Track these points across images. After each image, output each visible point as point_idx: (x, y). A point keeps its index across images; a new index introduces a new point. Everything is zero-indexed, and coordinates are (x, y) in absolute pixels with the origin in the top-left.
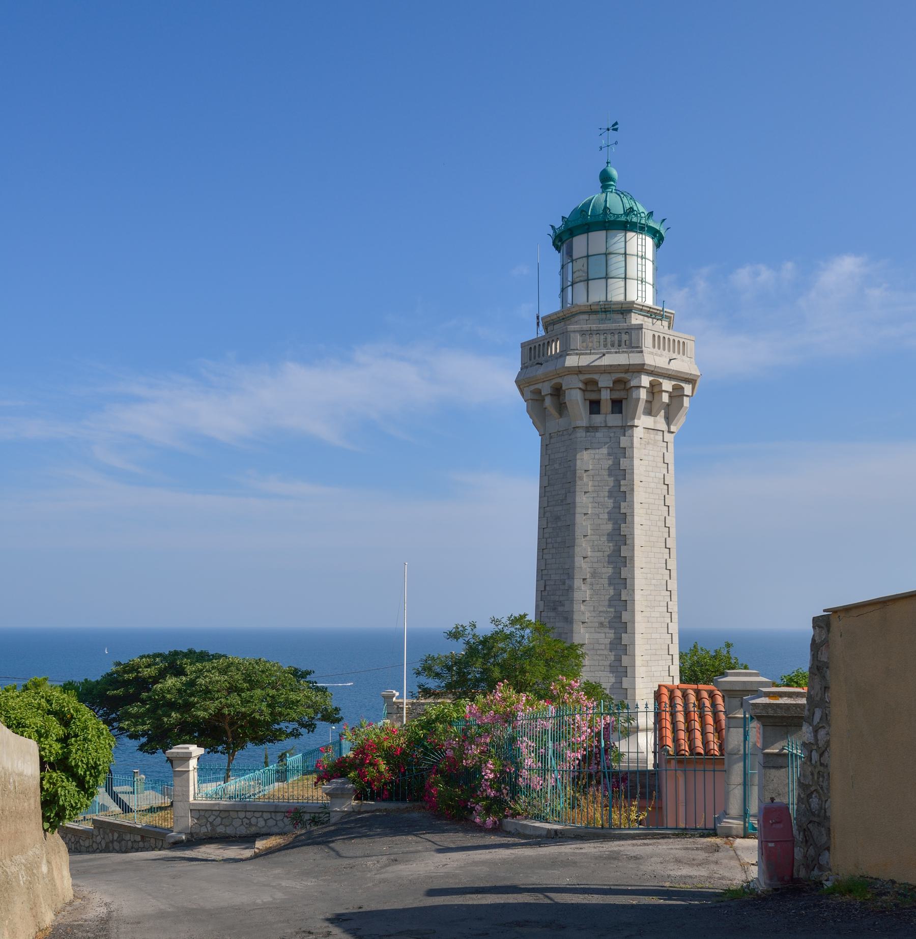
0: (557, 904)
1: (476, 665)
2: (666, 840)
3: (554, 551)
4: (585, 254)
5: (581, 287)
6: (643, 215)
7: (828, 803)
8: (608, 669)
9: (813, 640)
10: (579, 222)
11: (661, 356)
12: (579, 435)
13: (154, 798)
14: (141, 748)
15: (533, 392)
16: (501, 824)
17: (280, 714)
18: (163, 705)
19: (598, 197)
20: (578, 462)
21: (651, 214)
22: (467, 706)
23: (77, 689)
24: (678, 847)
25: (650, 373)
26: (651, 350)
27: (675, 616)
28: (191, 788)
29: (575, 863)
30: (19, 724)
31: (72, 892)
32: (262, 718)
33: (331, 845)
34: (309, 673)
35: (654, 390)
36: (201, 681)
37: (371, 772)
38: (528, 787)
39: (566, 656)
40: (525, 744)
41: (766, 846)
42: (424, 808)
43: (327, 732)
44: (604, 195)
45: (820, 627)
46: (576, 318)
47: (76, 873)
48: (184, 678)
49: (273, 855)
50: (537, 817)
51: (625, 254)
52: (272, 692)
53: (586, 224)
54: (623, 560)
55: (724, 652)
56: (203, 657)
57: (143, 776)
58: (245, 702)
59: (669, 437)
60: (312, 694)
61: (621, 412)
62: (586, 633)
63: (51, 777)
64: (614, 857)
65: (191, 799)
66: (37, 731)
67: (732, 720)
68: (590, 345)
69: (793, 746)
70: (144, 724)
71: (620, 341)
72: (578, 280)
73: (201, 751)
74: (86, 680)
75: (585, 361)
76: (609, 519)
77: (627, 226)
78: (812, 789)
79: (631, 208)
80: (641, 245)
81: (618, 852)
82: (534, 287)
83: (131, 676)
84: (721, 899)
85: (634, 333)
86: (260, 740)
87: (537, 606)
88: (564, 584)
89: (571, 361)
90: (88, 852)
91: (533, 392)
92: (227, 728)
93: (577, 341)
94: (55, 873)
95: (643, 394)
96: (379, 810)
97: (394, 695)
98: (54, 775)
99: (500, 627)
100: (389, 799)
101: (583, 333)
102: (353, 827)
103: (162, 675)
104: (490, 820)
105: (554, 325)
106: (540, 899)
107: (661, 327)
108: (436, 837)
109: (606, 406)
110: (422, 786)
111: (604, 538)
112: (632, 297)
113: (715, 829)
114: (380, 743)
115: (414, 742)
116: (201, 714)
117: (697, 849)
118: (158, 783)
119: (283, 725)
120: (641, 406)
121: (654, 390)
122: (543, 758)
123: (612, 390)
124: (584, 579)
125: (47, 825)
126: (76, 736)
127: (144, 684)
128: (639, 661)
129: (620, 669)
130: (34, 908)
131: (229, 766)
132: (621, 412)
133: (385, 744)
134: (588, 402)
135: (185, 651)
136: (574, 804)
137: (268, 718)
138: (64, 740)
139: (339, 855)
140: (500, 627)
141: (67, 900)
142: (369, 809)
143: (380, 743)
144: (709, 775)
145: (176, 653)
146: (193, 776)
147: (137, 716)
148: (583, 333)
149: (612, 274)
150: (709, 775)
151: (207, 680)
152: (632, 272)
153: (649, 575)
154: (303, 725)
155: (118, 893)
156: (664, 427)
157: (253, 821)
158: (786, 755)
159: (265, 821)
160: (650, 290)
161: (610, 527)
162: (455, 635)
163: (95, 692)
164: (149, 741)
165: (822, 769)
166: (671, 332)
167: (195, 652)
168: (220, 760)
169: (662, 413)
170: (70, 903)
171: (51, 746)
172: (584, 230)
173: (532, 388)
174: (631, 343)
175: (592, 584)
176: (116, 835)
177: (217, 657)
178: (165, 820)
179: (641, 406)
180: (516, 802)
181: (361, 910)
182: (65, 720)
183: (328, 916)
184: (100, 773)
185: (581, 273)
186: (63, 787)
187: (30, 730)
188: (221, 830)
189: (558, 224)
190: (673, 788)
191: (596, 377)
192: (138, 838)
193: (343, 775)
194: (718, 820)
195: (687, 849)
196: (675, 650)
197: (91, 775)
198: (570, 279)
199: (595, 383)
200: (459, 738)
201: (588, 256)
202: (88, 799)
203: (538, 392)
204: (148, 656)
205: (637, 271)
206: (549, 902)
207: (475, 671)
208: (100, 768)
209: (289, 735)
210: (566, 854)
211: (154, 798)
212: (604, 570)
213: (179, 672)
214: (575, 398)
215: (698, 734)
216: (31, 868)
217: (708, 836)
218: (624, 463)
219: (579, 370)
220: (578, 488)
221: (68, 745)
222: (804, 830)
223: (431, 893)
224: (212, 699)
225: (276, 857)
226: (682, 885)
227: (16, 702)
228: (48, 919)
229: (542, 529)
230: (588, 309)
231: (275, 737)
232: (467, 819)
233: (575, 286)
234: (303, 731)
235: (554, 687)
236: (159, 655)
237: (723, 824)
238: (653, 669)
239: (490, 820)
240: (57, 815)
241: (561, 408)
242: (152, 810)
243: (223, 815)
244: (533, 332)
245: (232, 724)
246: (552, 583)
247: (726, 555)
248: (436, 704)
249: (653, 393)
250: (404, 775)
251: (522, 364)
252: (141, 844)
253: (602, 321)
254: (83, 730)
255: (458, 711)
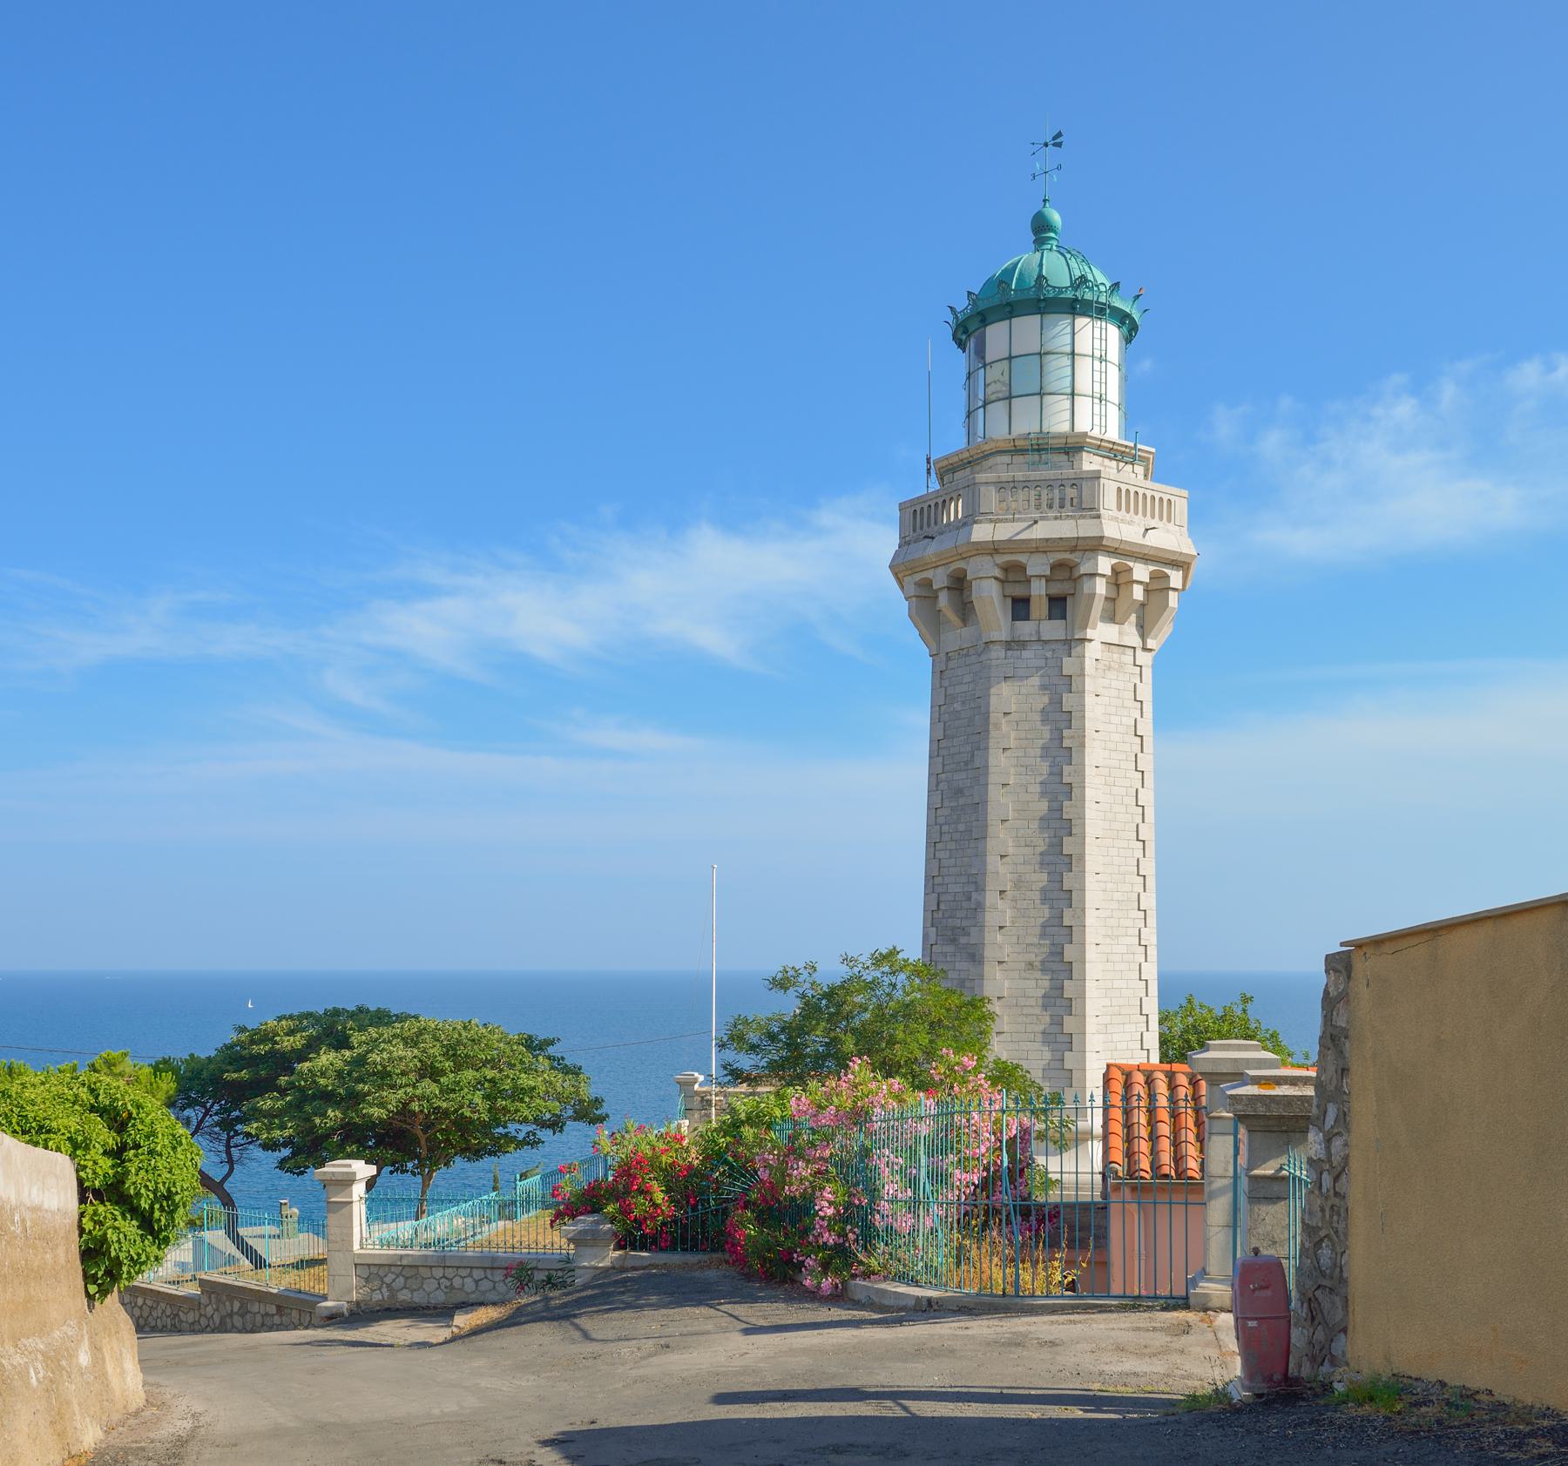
0: (914, 1417)
1: (814, 1034)
2: (1105, 1316)
3: (952, 846)
5: (998, 409)
6: (1102, 288)
7: (1345, 1257)
8: (1039, 1037)
9: (1326, 992)
10: (996, 301)
12: (994, 655)
13: (304, 1245)
14: (282, 1164)
15: (918, 584)
16: (845, 1289)
17: (505, 1110)
18: (314, 1097)
19: (1027, 259)
20: (993, 700)
21: (1116, 286)
22: (798, 1100)
23: (176, 1071)
24: (1123, 1326)
25: (1113, 552)
26: (1115, 513)
27: (1152, 952)
28: (356, 1230)
29: (953, 1351)
30: (41, 1127)
31: (143, 1396)
32: (476, 1116)
33: (576, 1321)
34: (551, 1043)
35: (1119, 579)
36: (374, 1057)
37: (640, 1206)
38: (889, 1230)
39: (965, 1017)
40: (887, 1163)
41: (1245, 1327)
42: (727, 1262)
43: (573, 1143)
44: (1038, 254)
45: (1336, 971)
46: (991, 461)
47: (145, 1364)
48: (347, 1053)
49: (479, 1337)
50: (902, 1278)
51: (1073, 353)
52: (490, 1074)
53: (1008, 304)
54: (1067, 860)
55: (1238, 1012)
56: (381, 1018)
57: (296, 1210)
58: (446, 1091)
59: (1145, 659)
60: (558, 1079)
61: (1064, 617)
62: (1006, 982)
63: (95, 1213)
64: (1017, 1342)
65: (356, 1247)
66: (69, 1139)
67: (1215, 1122)
68: (1014, 505)
69: (1295, 1164)
70: (283, 1127)
71: (1062, 500)
72: (993, 397)
73: (372, 1170)
74: (192, 1055)
75: (1004, 532)
76: (1043, 794)
77: (1075, 307)
78: (1322, 1233)
79: (1082, 276)
80: (1096, 338)
81: (1025, 1335)
82: (931, 409)
83: (262, 1049)
84: (1171, 1410)
85: (1085, 486)
86: (476, 1153)
87: (925, 936)
88: (969, 899)
89: (981, 532)
90: (193, 1332)
91: (918, 584)
92: (420, 1133)
93: (990, 499)
94: (110, 1367)
95: (1101, 587)
96: (655, 1266)
97: (695, 1081)
98: (101, 1209)
99: (856, 970)
100: (673, 1248)
101: (1001, 486)
102: (611, 1293)
103: (312, 1046)
104: (827, 1283)
105: (956, 472)
106: (889, 1410)
107: (1133, 475)
108: (741, 1310)
109: (1039, 607)
110: (725, 1229)
111: (1035, 825)
112: (1083, 425)
113: (1187, 1298)
114: (655, 1157)
115: (713, 1156)
116: (376, 1112)
117: (1155, 1329)
118: (313, 1223)
119: (512, 1128)
120: (1098, 607)
121: (1119, 579)
122: (913, 1182)
123: (1048, 580)
124: (1002, 892)
125: (93, 1289)
126: (137, 1146)
127: (285, 1061)
128: (1091, 1025)
129: (1060, 1038)
130: (59, 1421)
131: (423, 1193)
132: (1064, 617)
133: (664, 1158)
134: (1009, 601)
135: (351, 1008)
136: (960, 1256)
137: (485, 1117)
138: (117, 1153)
139: (586, 1336)
140: (856, 970)
141: (132, 1409)
142: (638, 1264)
143: (655, 1157)
144: (1179, 1210)
145: (336, 1013)
146: (359, 1211)
147: (270, 1114)
148: (1001, 486)
149: (1048, 389)
150: (1179, 1210)
151: (385, 1055)
152: (1083, 384)
153: (1110, 886)
154: (544, 1125)
155: (226, 1393)
156: (1135, 641)
157: (457, 1282)
158: (1283, 1178)
159: (477, 1282)
160: (1114, 415)
161: (1044, 806)
162: (782, 983)
163: (205, 1074)
164: (294, 1154)
165: (1336, 1201)
166: (1149, 484)
167: (368, 1011)
168: (406, 1184)
169: (1133, 618)
170: (136, 1414)
171: (95, 1163)
172: (1003, 309)
173: (918, 577)
174: (1081, 502)
175: (1015, 900)
176: (237, 1305)
177: (401, 1018)
178: (319, 1280)
179: (1098, 607)
180: (870, 1255)
181: (592, 1427)
182: (118, 1121)
183: (549, 1434)
184: (177, 1206)
185: (998, 387)
186: (115, 1228)
187: (57, 1137)
188: (404, 1296)
189: (962, 304)
190: (1125, 1230)
191: (1022, 558)
192: (273, 1309)
193: (595, 1210)
194: (1193, 1283)
195: (1138, 1329)
196: (1152, 1007)
197: (162, 1209)
198: (981, 396)
199: (1021, 568)
200: (779, 1149)
201: (1010, 358)
202: (159, 1248)
203: (927, 584)
204: (291, 1017)
205: (1092, 380)
206: (904, 1414)
207: (816, 1040)
208: (177, 1198)
209: (520, 1144)
210: (941, 1336)
211: (304, 1245)
212: (1035, 877)
213: (342, 1043)
214: (989, 595)
215: (1165, 1144)
216: (56, 1360)
217: (1175, 1308)
218: (1068, 701)
219: (994, 548)
220: (992, 743)
221: (123, 1162)
222: (1310, 1301)
223: (721, 1399)
224: (392, 1087)
225: (479, 1341)
226: (1123, 1389)
227: (37, 1089)
228: (90, 1436)
229: (933, 810)
230: (1010, 446)
231: (497, 1147)
232: (793, 1281)
233: (989, 407)
234: (545, 1134)
235: (937, 1071)
236: (308, 1015)
237: (1198, 1290)
238: (1116, 1037)
239: (827, 1283)
240: (108, 1273)
241: (965, 610)
242: (302, 1264)
243: (407, 1272)
244: (924, 486)
245: (428, 1126)
246: (950, 898)
247: (1214, 848)
248: (753, 1094)
249: (1118, 586)
250: (694, 1208)
251: (901, 538)
252: (277, 1319)
253: (1033, 466)
254: (147, 1137)
255: (783, 1107)
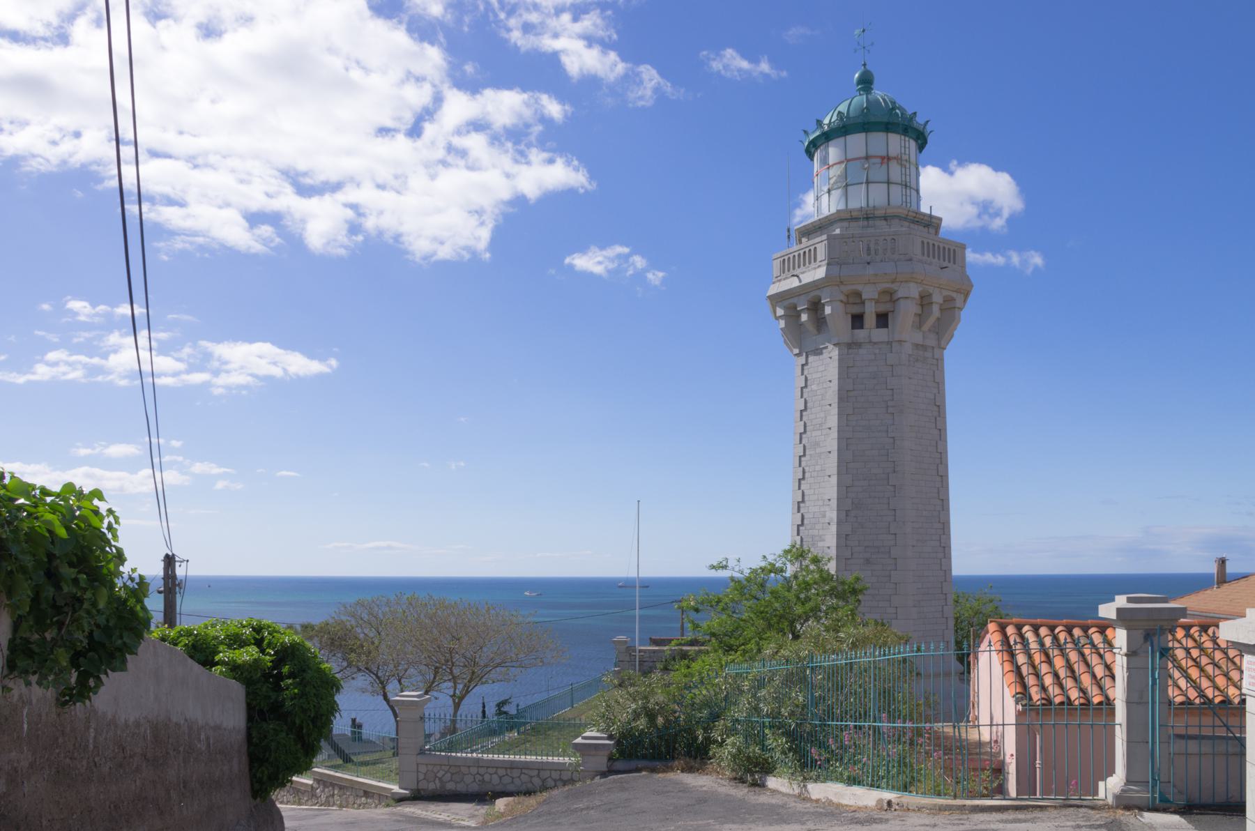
4: (863, 154)
11: (930, 264)
109: (870, 320)
123: (877, 302)
157: (487, 777)
188: (450, 786)
199: (858, 294)
230: (848, 216)
